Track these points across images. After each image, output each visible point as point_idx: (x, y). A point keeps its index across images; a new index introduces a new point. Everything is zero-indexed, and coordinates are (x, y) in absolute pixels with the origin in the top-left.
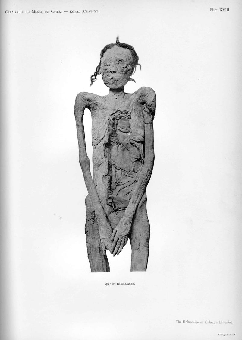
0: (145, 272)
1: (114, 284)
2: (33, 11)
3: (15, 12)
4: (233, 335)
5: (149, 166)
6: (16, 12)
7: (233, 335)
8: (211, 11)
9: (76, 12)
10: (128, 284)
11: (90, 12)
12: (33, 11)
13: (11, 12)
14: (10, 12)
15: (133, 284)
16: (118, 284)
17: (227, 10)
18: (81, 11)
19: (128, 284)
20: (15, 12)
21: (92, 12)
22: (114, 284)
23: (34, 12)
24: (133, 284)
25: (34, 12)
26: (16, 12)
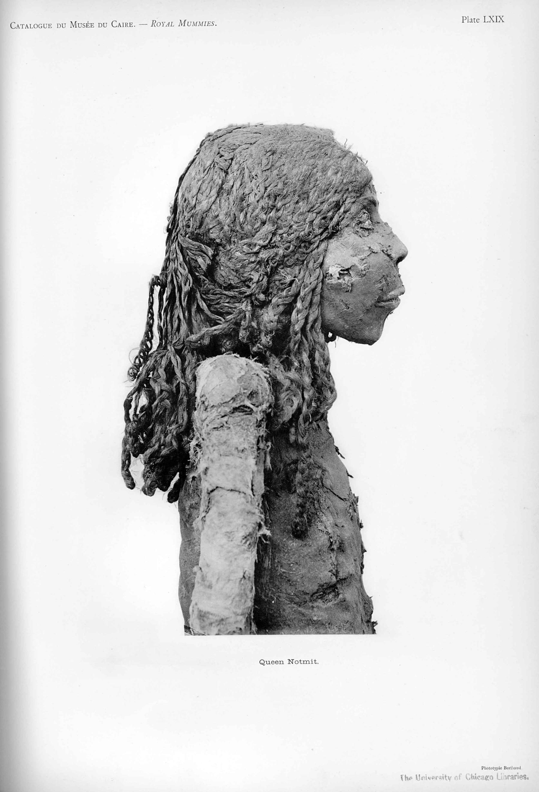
0: (367, 638)
1: (281, 662)
2: (74, 23)
3: (32, 26)
4: (517, 768)
5: (221, 431)
6: (36, 26)
7: (517, 768)
8: (465, 21)
9: (165, 25)
10: (305, 662)
11: (195, 24)
12: (74, 23)
13: (24, 27)
14: (21, 27)
15: (263, 663)
16: (291, 661)
17: (499, 19)
18: (176, 23)
19: (305, 662)
20: (32, 26)
21: (201, 24)
22: (281, 662)
23: (74, 25)
24: (263, 663)
25: (74, 25)
26: (36, 26)
